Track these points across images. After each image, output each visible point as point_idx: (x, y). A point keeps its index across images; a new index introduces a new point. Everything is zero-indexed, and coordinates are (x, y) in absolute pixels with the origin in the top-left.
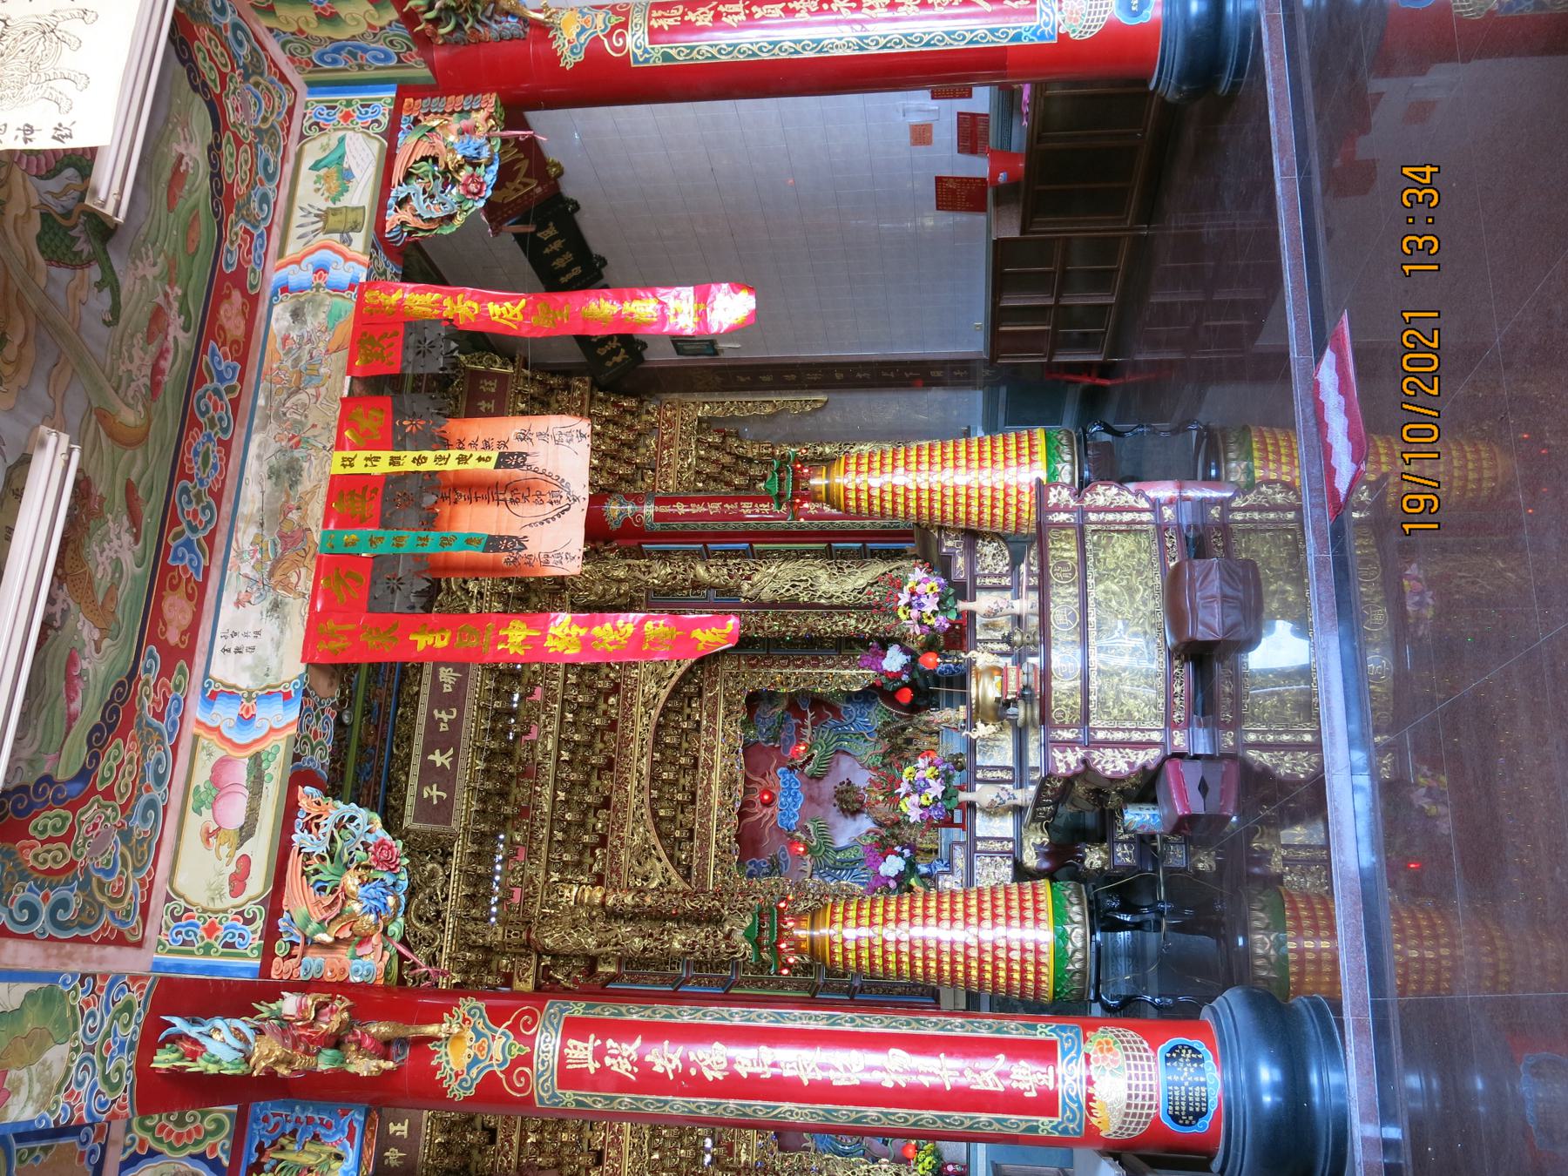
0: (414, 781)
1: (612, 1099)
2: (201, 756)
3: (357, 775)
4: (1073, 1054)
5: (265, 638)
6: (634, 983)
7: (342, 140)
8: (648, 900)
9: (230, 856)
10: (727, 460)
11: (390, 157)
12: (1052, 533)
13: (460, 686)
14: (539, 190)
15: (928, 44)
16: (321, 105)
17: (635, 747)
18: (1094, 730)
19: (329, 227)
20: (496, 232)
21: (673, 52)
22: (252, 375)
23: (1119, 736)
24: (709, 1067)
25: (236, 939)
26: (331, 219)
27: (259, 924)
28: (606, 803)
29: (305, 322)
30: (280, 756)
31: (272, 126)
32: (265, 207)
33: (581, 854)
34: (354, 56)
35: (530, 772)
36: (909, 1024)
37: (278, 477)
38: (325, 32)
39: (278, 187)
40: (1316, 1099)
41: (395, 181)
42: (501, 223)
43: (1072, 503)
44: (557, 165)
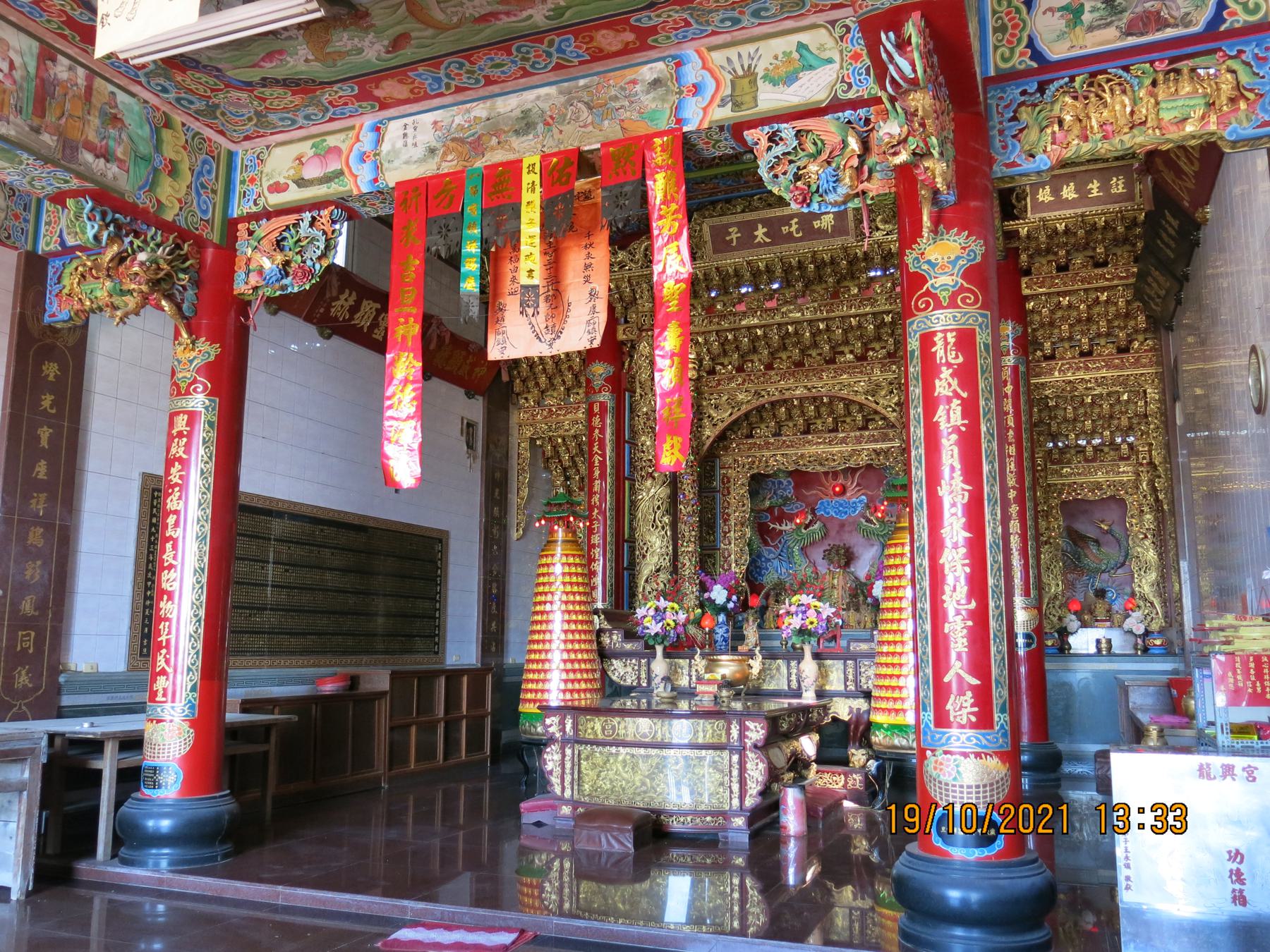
0: (739, 218)
2: (342, 136)
4: (984, 742)
7: (830, 61)
11: (815, 112)
12: (722, 723)
13: (821, 233)
23: (568, 765)
26: (747, 80)
27: (254, 209)
28: (769, 367)
30: (342, 189)
36: (997, 607)
37: (523, 118)
40: (154, 851)
43: (749, 743)
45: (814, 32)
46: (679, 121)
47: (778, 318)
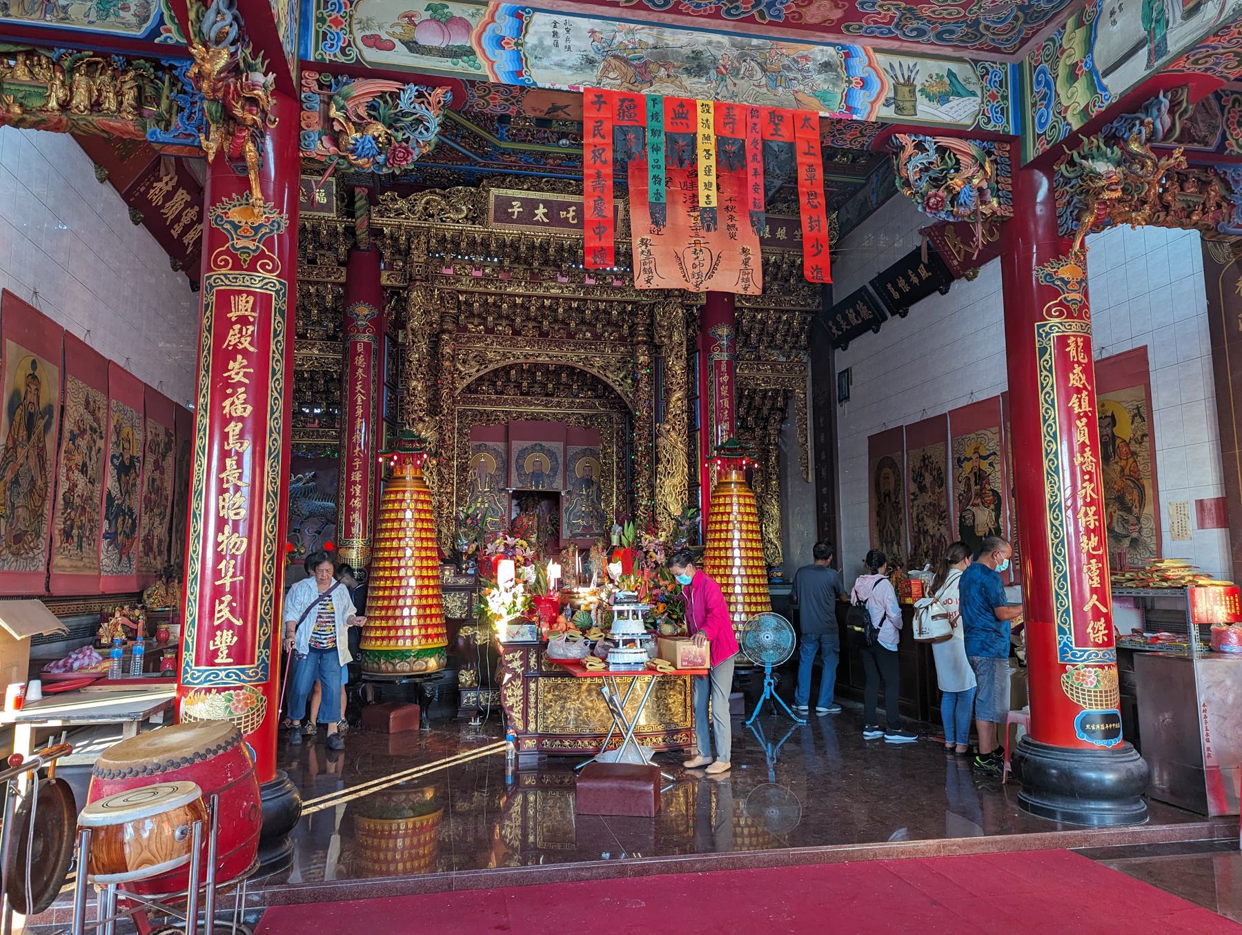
1: (209, 331)
3: (524, 152)
5: (565, 55)
6: (390, 355)
7: (973, 94)
8: (447, 364)
9: (393, 35)
10: (765, 412)
14: (955, 263)
15: (1055, 559)
16: (1003, 76)
17: (555, 352)
18: (536, 681)
19: (900, 88)
20: (921, 232)
21: (1047, 357)
22: (776, 32)
23: (532, 699)
24: (233, 403)
25: (329, 42)
26: (907, 89)
27: (342, 59)
28: (516, 333)
29: (820, 73)
30: (473, 71)
31: (983, 35)
32: (914, 33)
33: (479, 316)
34: (1043, 99)
35: (535, 278)
38: (1062, 71)
39: (933, 44)
41: (938, 139)
42: (929, 235)
44: (975, 276)
45: (962, 65)
46: (849, 108)
47: (540, 292)
